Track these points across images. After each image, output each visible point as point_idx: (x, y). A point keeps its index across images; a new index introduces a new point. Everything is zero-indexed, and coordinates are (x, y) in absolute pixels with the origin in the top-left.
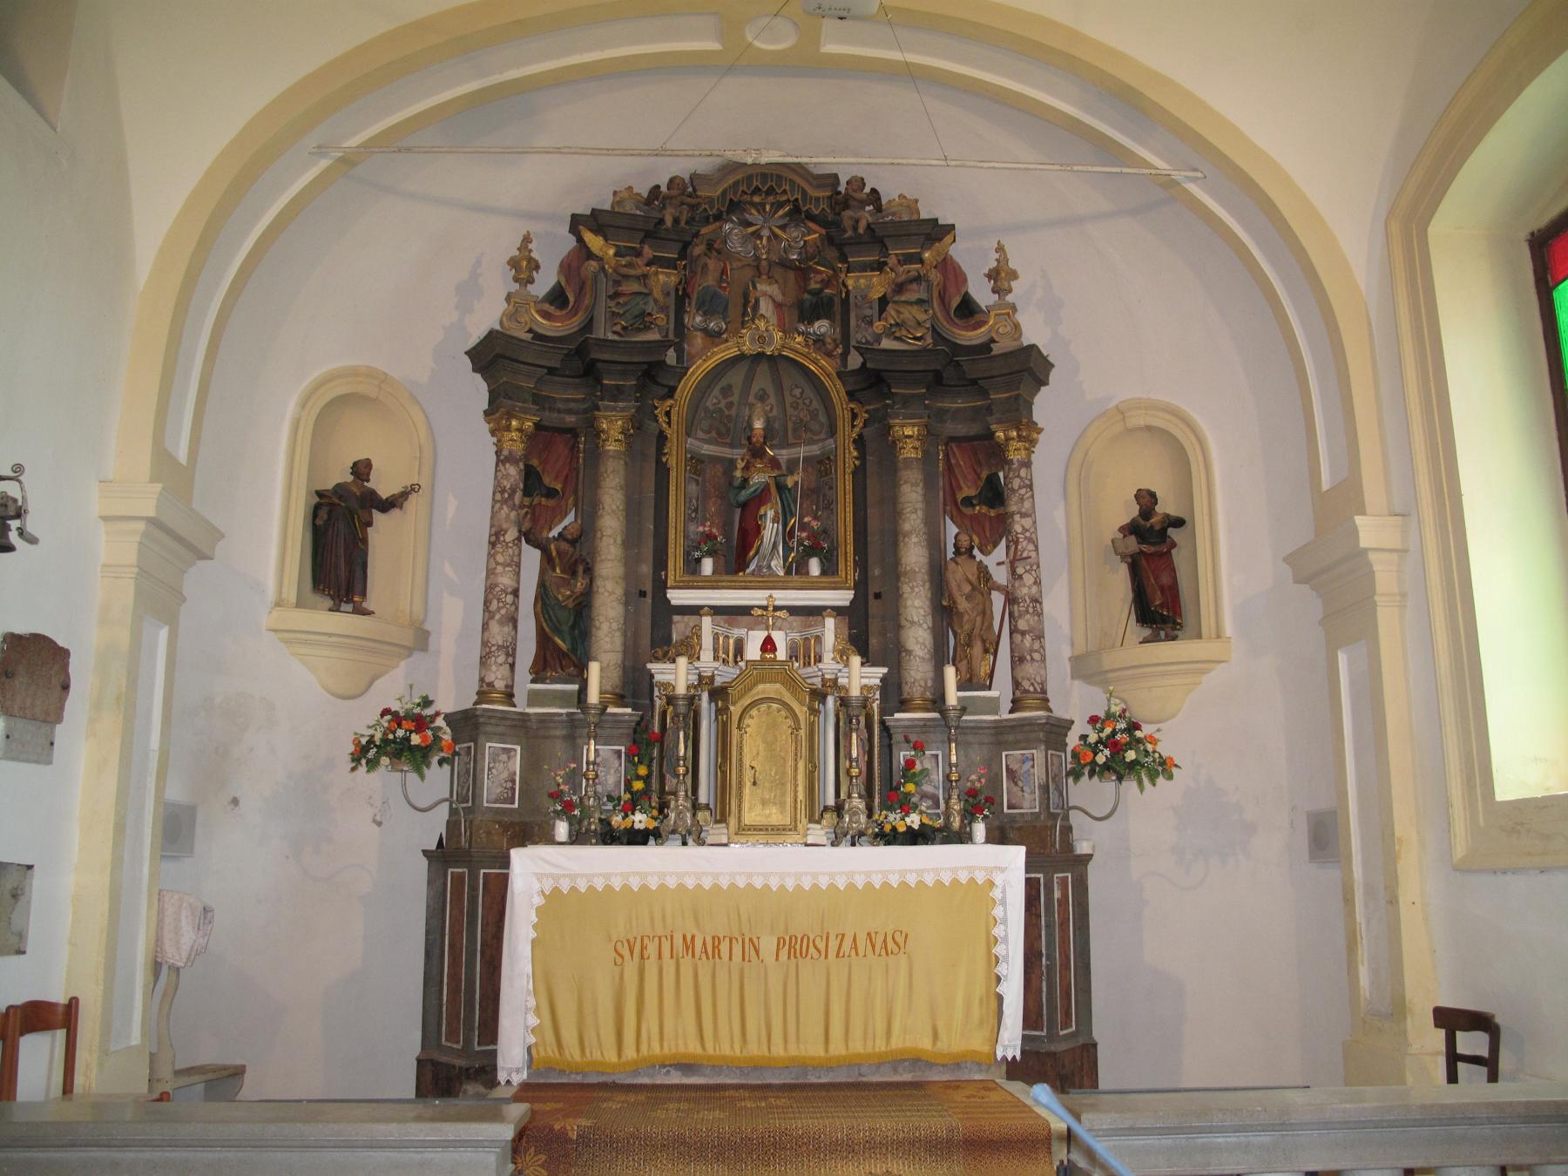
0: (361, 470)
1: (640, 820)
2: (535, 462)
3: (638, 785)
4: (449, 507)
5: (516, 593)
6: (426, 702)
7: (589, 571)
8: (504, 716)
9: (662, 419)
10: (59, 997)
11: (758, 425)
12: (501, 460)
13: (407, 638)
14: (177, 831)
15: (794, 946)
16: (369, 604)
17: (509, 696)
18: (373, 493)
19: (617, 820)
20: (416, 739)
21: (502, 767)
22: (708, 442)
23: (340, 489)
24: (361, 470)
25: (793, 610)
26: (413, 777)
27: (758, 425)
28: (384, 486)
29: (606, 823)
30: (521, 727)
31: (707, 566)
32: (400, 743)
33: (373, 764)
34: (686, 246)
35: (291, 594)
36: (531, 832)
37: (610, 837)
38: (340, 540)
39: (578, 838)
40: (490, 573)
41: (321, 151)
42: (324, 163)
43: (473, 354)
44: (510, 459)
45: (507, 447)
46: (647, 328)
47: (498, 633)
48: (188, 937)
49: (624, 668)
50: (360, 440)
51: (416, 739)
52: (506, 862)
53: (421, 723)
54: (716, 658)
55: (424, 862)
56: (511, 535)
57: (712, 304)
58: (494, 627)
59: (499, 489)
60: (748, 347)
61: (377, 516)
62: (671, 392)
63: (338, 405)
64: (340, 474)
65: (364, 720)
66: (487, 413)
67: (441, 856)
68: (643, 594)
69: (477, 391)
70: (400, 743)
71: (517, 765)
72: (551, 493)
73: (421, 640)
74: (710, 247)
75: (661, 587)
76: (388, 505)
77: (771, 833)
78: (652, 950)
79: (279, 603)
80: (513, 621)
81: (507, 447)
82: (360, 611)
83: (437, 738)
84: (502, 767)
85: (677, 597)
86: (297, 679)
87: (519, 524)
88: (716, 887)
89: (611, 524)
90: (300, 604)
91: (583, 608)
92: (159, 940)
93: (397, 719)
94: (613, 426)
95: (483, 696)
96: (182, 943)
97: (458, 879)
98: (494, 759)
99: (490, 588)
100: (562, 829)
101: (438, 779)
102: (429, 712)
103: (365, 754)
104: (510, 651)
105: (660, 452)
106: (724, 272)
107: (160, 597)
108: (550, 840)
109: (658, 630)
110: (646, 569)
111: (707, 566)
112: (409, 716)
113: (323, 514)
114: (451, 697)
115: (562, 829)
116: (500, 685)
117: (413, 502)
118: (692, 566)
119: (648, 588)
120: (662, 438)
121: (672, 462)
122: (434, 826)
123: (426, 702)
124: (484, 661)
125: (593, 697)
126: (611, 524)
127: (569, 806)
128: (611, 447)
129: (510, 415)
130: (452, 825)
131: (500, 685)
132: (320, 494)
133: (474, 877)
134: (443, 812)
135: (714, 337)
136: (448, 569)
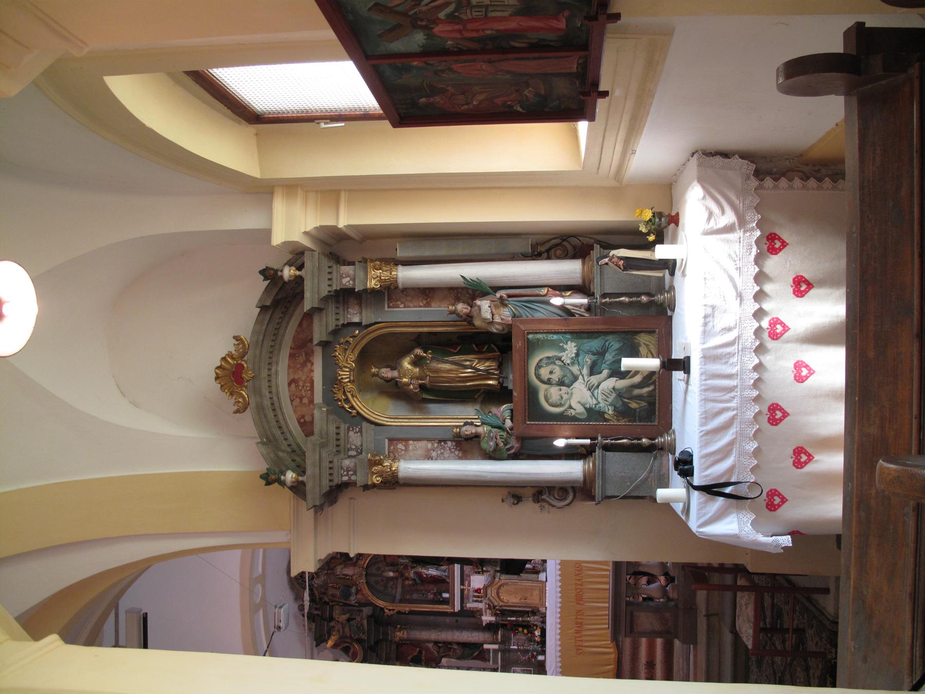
1: (537, 633)
2: (409, 658)
3: (525, 631)
7: (450, 643)
9: (392, 612)
11: (391, 574)
15: (579, 599)
22: (396, 588)
25: (462, 583)
27: (391, 574)
31: (446, 595)
34: (326, 603)
37: (543, 643)
46: (362, 625)
54: (481, 602)
57: (347, 594)
60: (363, 580)
62: (382, 609)
68: (457, 621)
72: (420, 652)
74: (325, 594)
75: (454, 614)
77: (543, 592)
78: (580, 643)
85: (457, 608)
88: (560, 581)
89: (434, 635)
91: (464, 645)
94: (400, 635)
100: (540, 658)
105: (405, 613)
106: (333, 587)
109: (469, 618)
110: (448, 620)
111: (446, 595)
115: (540, 658)
118: (446, 602)
119: (454, 619)
120: (399, 613)
121: (407, 609)
125: (496, 647)
126: (434, 635)
127: (533, 656)
128: (405, 636)
135: (358, 591)
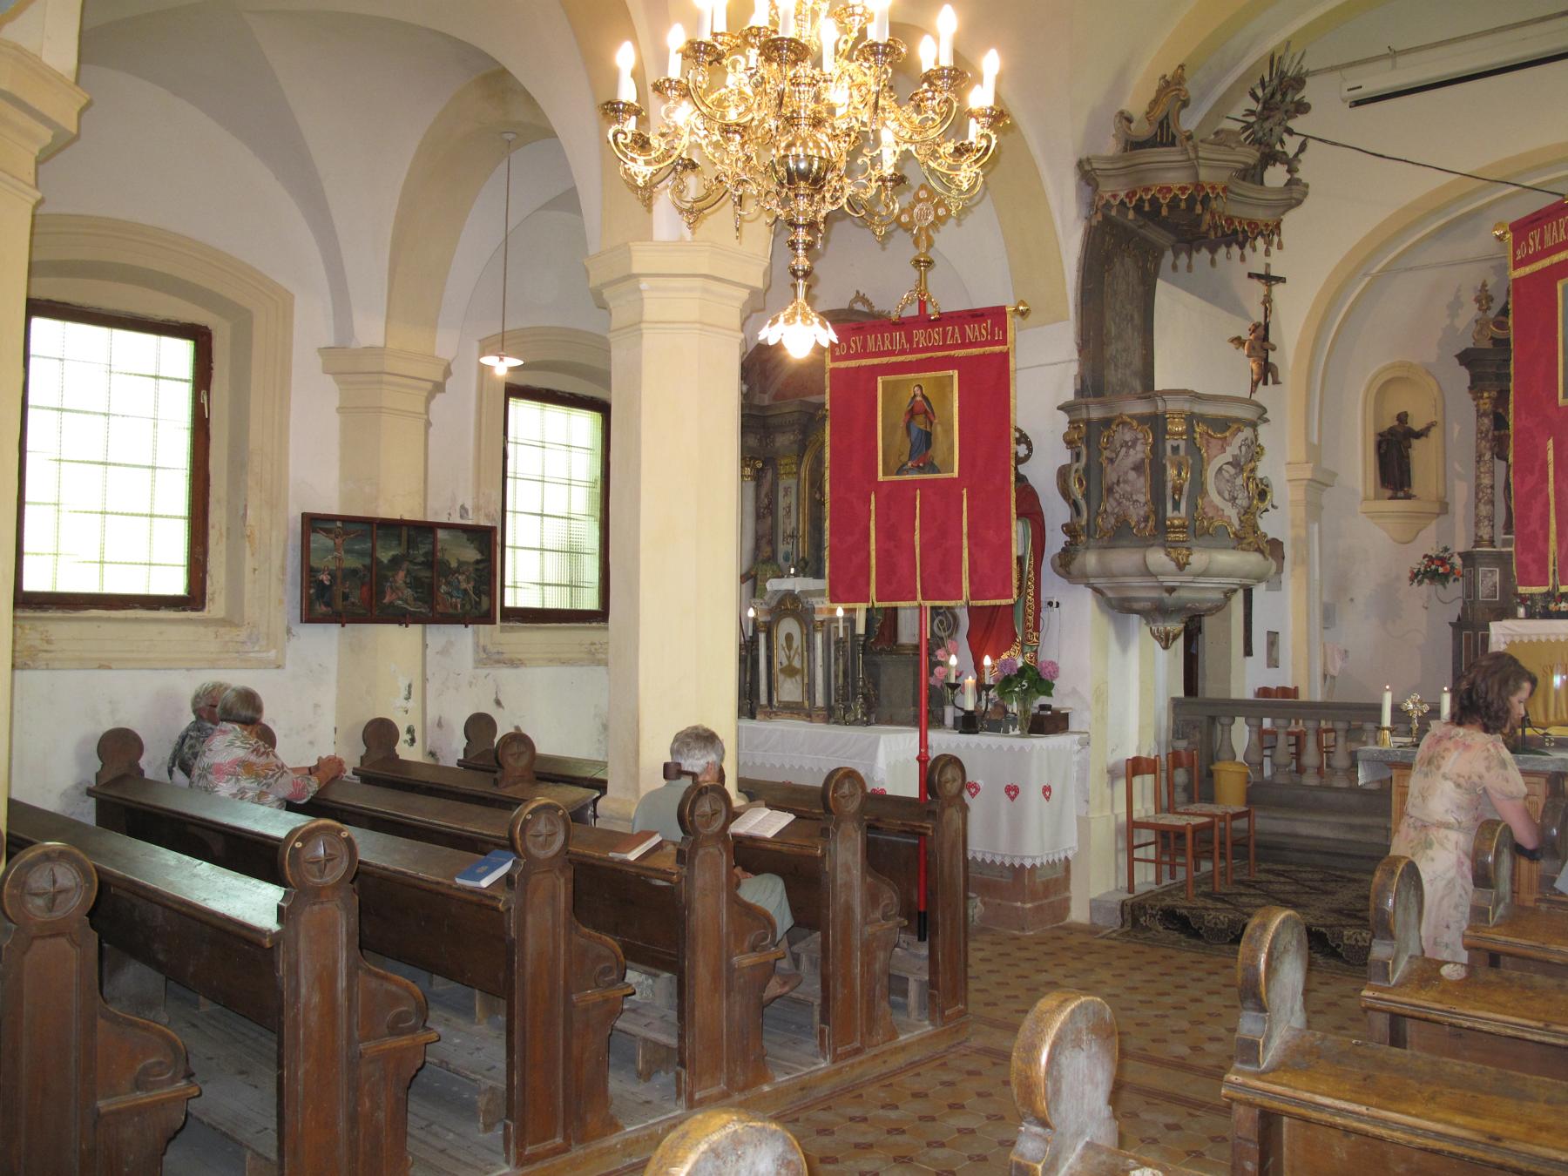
0: (1402, 418)
4: (1456, 430)
5: (1492, 487)
6: (1446, 550)
8: (1489, 553)
10: (1290, 685)
12: (1480, 415)
13: (1436, 508)
14: (1329, 616)
16: (1415, 490)
17: (1492, 543)
18: (1410, 429)
19: (1552, 606)
20: (1441, 570)
21: (1489, 580)
23: (1391, 430)
24: (1402, 418)
26: (1440, 587)
28: (1416, 424)
29: (1546, 608)
30: (1502, 560)
32: (1434, 571)
33: (1420, 583)
35: (1371, 493)
36: (1505, 613)
38: (1394, 458)
39: (1530, 615)
40: (1478, 477)
41: (1365, 275)
42: (1367, 279)
43: (1458, 356)
44: (1485, 414)
45: (1482, 408)
47: (1484, 510)
48: (1339, 663)
49: (1018, 872)
50: (1401, 401)
51: (1441, 570)
52: (1487, 628)
53: (1443, 561)
55: (1450, 629)
56: (1488, 456)
58: (1482, 507)
59: (1479, 431)
61: (1415, 442)
63: (1385, 388)
64: (1390, 422)
65: (1416, 561)
66: (1471, 389)
67: (1459, 626)
69: (1464, 375)
70: (1434, 571)
71: (1497, 578)
73: (1444, 508)
76: (1418, 435)
79: (1365, 499)
80: (1492, 502)
81: (1482, 408)
82: (1408, 497)
83: (1452, 568)
84: (1489, 580)
86: (1377, 538)
87: (1491, 449)
90: (1377, 497)
92: (1325, 664)
93: (1431, 559)
95: (1478, 543)
96: (1336, 668)
97: (1468, 637)
98: (1485, 575)
99: (1478, 486)
100: (1521, 611)
101: (1455, 589)
102: (1447, 555)
103: (1416, 576)
104: (1491, 518)
107: (1314, 510)
108: (1514, 616)
112: (1438, 558)
113: (1384, 446)
114: (1461, 543)
115: (1521, 611)
116: (1486, 537)
117: (1434, 433)
122: (1454, 612)
123: (1446, 550)
124: (1477, 525)
129: (1482, 391)
130: (1464, 610)
131: (1486, 537)
132: (1381, 435)
133: (1476, 634)
134: (1460, 603)
136: (1457, 466)
